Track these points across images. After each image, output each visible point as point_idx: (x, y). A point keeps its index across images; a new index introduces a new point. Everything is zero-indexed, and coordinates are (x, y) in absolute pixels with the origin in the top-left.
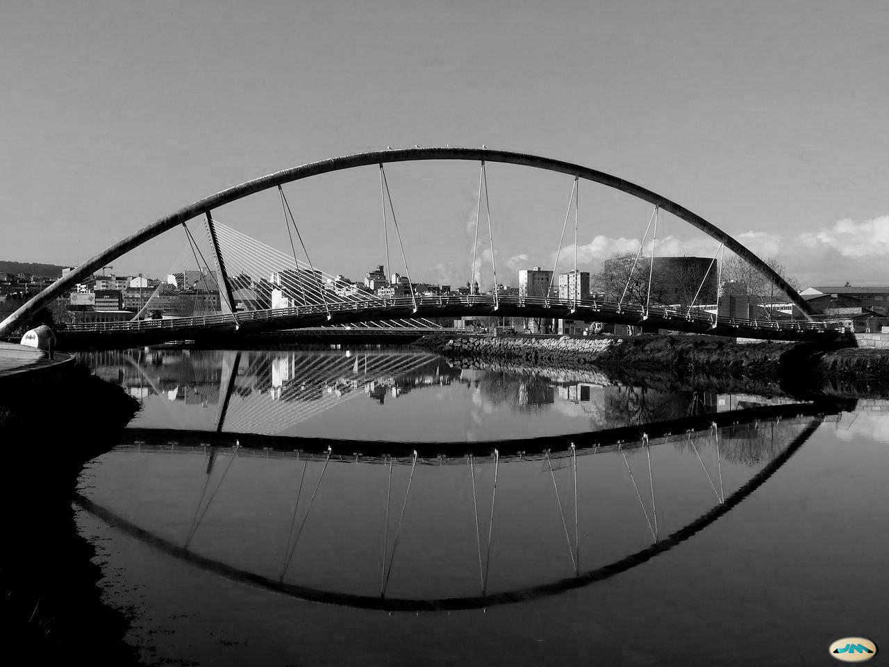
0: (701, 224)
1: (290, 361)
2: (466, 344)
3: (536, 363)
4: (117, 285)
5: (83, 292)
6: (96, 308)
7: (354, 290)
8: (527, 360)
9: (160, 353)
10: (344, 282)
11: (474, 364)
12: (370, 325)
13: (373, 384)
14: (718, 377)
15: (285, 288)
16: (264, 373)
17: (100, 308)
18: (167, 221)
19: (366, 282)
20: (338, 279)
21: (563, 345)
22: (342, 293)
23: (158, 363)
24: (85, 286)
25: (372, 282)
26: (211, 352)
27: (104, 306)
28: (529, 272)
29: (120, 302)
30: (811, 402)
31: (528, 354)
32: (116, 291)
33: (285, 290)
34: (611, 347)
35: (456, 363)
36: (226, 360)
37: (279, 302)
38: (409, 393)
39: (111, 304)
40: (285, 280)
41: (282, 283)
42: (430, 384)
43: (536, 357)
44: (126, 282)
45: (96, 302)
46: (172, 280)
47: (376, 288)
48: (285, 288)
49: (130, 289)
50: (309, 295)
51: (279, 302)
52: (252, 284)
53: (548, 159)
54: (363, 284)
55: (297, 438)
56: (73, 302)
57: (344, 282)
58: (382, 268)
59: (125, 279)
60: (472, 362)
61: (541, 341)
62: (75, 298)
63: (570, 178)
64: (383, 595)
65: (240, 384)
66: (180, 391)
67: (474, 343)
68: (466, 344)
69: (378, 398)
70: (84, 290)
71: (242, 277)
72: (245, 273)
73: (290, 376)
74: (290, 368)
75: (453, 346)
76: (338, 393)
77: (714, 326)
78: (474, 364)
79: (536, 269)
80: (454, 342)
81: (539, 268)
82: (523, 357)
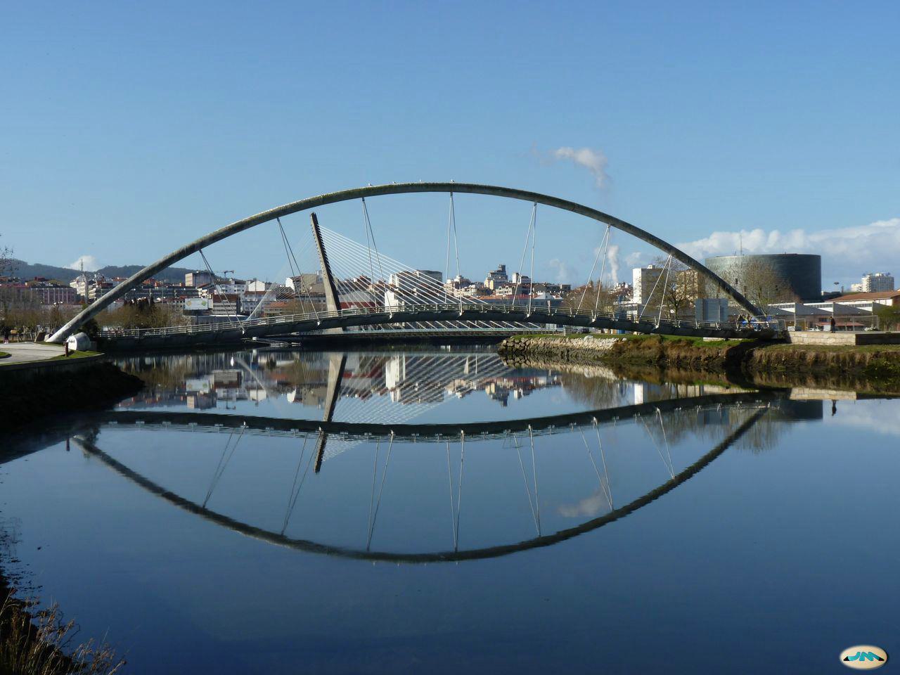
0: (650, 239)
1: (401, 364)
2: (518, 343)
3: (568, 360)
5: (204, 297)
6: (216, 312)
7: (472, 291)
8: (562, 358)
9: (273, 355)
10: (464, 283)
11: (525, 362)
13: (493, 386)
14: (685, 369)
16: (377, 373)
17: (219, 312)
18: (187, 249)
19: (486, 283)
20: (457, 280)
21: (586, 344)
22: (459, 294)
23: (272, 365)
25: (492, 282)
26: (318, 354)
27: (222, 310)
28: (642, 270)
29: (238, 306)
30: (757, 391)
31: (562, 353)
32: (235, 295)
34: (615, 345)
35: (509, 361)
36: (333, 361)
38: (531, 395)
40: (403, 283)
42: (543, 385)
43: (568, 355)
44: (245, 286)
45: (214, 306)
46: (289, 284)
47: (495, 288)
49: (248, 293)
52: (370, 286)
53: (509, 189)
54: (482, 284)
55: (263, 418)
56: (187, 308)
57: (464, 283)
58: (504, 267)
60: (523, 360)
61: (572, 340)
62: (190, 304)
63: (529, 204)
64: (368, 549)
66: (298, 392)
67: (525, 343)
68: (518, 343)
69: (500, 399)
70: (204, 295)
71: (362, 279)
72: (365, 275)
73: (401, 378)
74: (401, 372)
75: (506, 346)
76: (459, 395)
77: (657, 327)
78: (525, 362)
79: (650, 267)
80: (507, 342)
81: (654, 266)
82: (559, 355)
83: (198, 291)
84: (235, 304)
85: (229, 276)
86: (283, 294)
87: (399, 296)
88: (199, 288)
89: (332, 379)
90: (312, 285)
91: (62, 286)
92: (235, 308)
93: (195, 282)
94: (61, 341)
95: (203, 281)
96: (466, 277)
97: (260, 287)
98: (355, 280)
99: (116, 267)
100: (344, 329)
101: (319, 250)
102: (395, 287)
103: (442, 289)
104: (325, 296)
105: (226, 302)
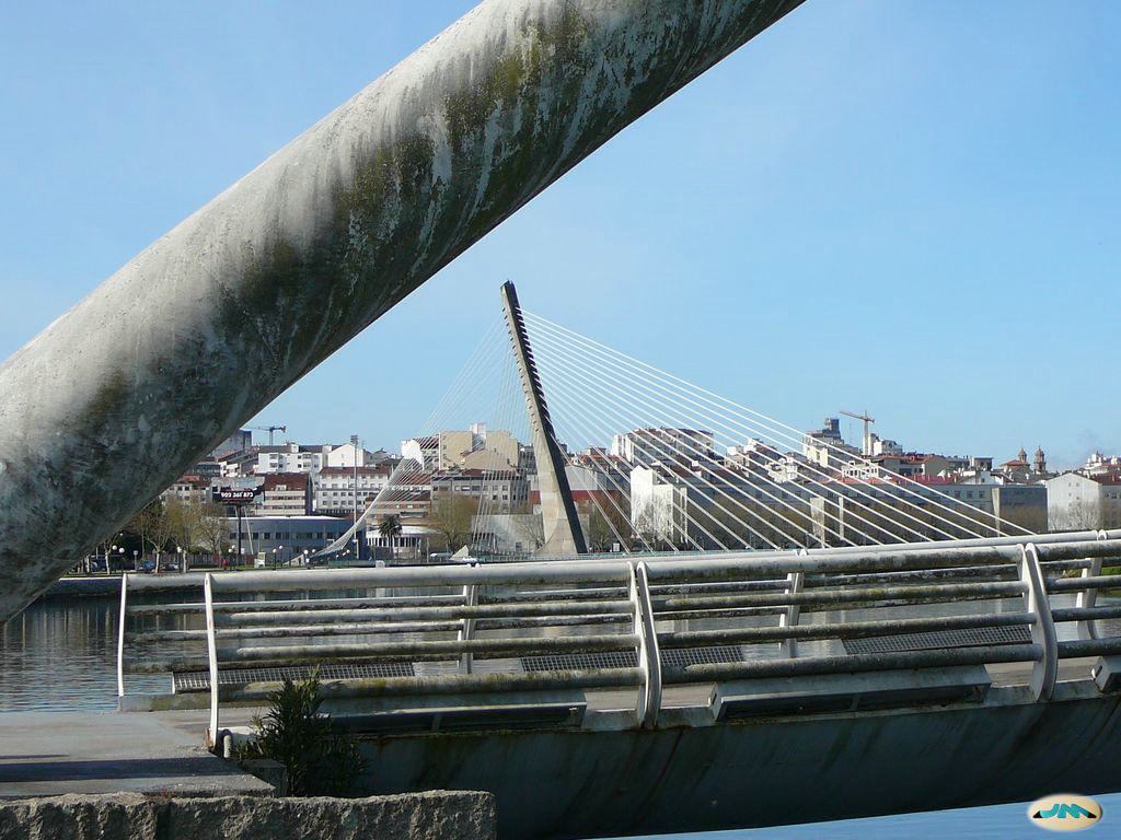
4: (301, 462)
15: (658, 463)
18: (159, 366)
24: (236, 465)
29: (309, 498)
33: (659, 469)
39: (290, 503)
41: (636, 452)
48: (658, 463)
49: (328, 471)
58: (835, 423)
59: (319, 449)
83: (219, 467)
84: (303, 493)
88: (220, 460)
90: (466, 454)
92: (303, 503)
105: (281, 491)
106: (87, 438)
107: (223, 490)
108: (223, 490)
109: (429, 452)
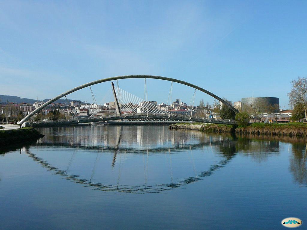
12: (161, 120)
15: (141, 107)
19: (172, 105)
22: (162, 109)
25: (174, 105)
29: (88, 112)
37: (139, 111)
47: (175, 107)
50: (149, 109)
51: (139, 111)
57: (164, 106)
58: (178, 100)
65: (174, 131)
85: (85, 102)
86: (103, 108)
87: (141, 110)
89: (118, 137)
91: (30, 106)
93: (74, 104)
94: (21, 125)
95: (77, 104)
96: (165, 104)
97: (95, 106)
98: (128, 104)
99: (20, 98)
100: (122, 121)
101: (114, 94)
102: (141, 106)
103: (157, 107)
104: (116, 109)
105: (84, 111)
106: (143, 111)
107: (71, 112)
108: (71, 112)
109: (108, 105)
